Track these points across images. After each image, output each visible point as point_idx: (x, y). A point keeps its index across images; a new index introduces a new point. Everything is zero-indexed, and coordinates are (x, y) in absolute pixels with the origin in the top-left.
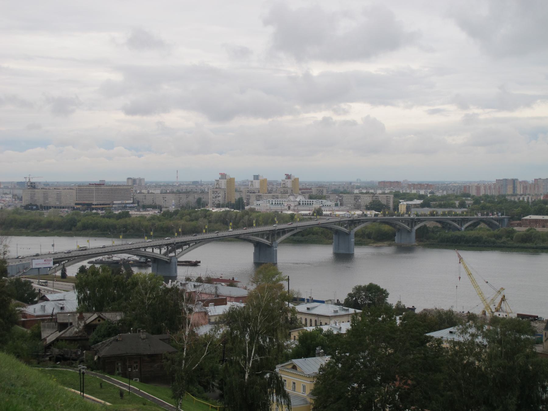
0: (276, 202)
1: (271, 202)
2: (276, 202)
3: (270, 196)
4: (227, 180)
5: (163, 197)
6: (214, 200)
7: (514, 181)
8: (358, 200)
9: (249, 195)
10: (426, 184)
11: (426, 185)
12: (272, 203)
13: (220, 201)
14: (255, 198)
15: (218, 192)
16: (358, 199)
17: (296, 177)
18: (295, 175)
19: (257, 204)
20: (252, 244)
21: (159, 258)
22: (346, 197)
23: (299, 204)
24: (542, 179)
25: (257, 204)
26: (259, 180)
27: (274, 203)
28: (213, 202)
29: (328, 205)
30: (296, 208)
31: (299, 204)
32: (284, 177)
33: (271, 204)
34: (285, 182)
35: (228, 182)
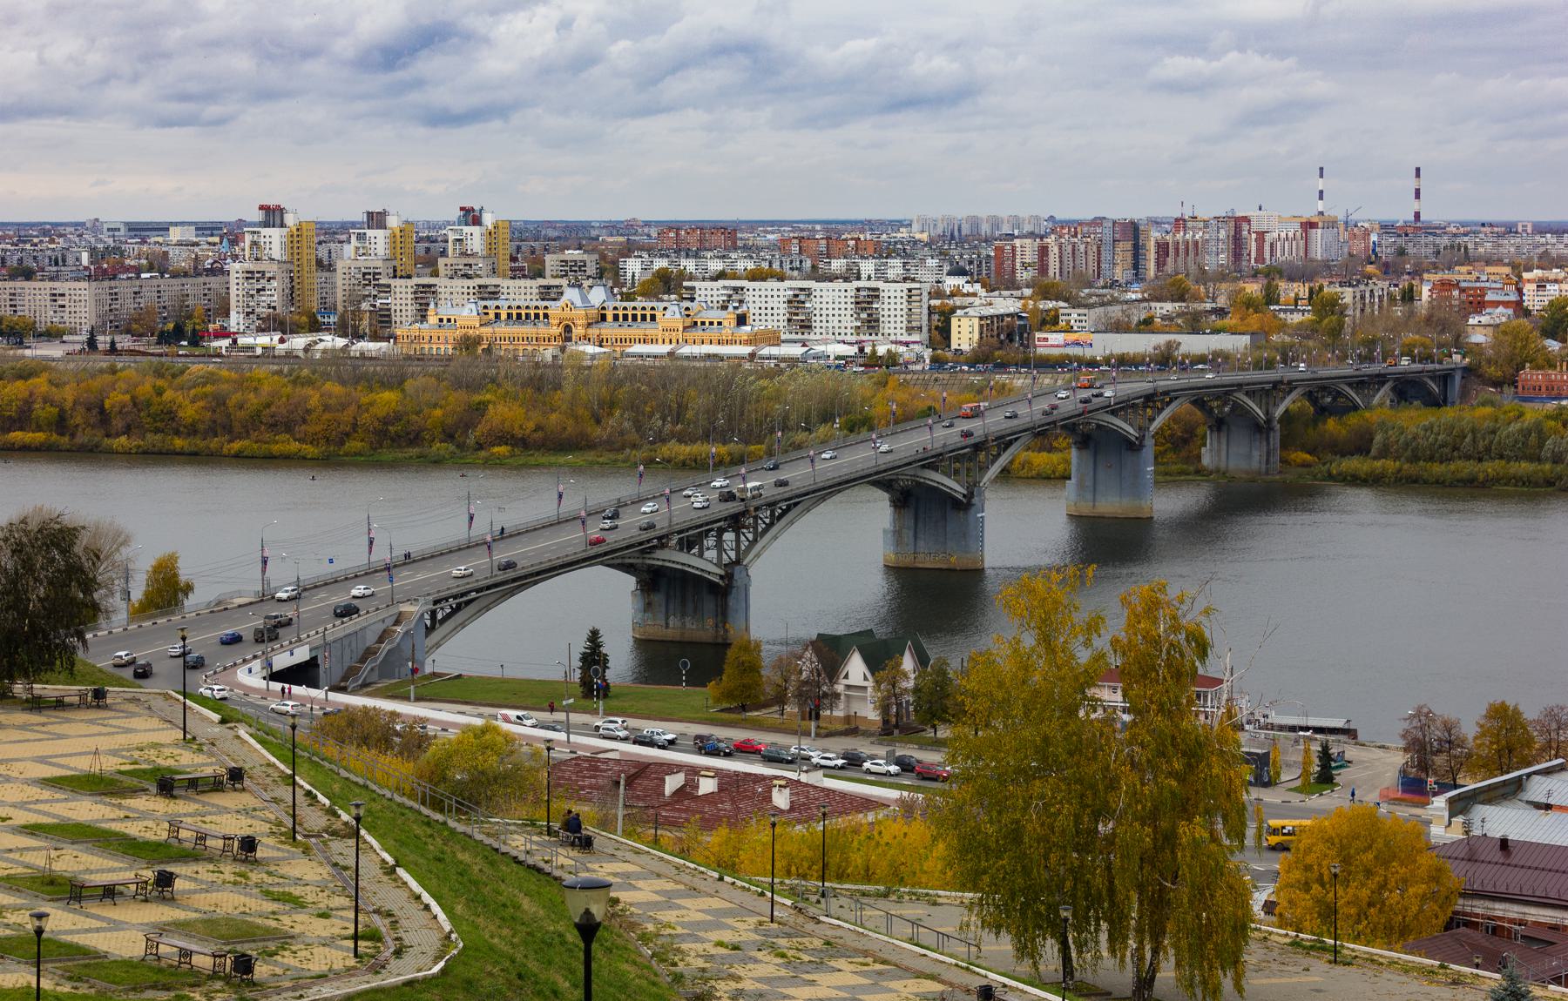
2: (514, 312)
5: (55, 295)
7: (1133, 231)
9: (389, 286)
13: (274, 308)
14: (410, 296)
15: (267, 275)
16: (802, 298)
19: (441, 320)
20: (886, 496)
21: (679, 567)
24: (1204, 213)
25: (441, 320)
26: (282, 225)
30: (593, 332)
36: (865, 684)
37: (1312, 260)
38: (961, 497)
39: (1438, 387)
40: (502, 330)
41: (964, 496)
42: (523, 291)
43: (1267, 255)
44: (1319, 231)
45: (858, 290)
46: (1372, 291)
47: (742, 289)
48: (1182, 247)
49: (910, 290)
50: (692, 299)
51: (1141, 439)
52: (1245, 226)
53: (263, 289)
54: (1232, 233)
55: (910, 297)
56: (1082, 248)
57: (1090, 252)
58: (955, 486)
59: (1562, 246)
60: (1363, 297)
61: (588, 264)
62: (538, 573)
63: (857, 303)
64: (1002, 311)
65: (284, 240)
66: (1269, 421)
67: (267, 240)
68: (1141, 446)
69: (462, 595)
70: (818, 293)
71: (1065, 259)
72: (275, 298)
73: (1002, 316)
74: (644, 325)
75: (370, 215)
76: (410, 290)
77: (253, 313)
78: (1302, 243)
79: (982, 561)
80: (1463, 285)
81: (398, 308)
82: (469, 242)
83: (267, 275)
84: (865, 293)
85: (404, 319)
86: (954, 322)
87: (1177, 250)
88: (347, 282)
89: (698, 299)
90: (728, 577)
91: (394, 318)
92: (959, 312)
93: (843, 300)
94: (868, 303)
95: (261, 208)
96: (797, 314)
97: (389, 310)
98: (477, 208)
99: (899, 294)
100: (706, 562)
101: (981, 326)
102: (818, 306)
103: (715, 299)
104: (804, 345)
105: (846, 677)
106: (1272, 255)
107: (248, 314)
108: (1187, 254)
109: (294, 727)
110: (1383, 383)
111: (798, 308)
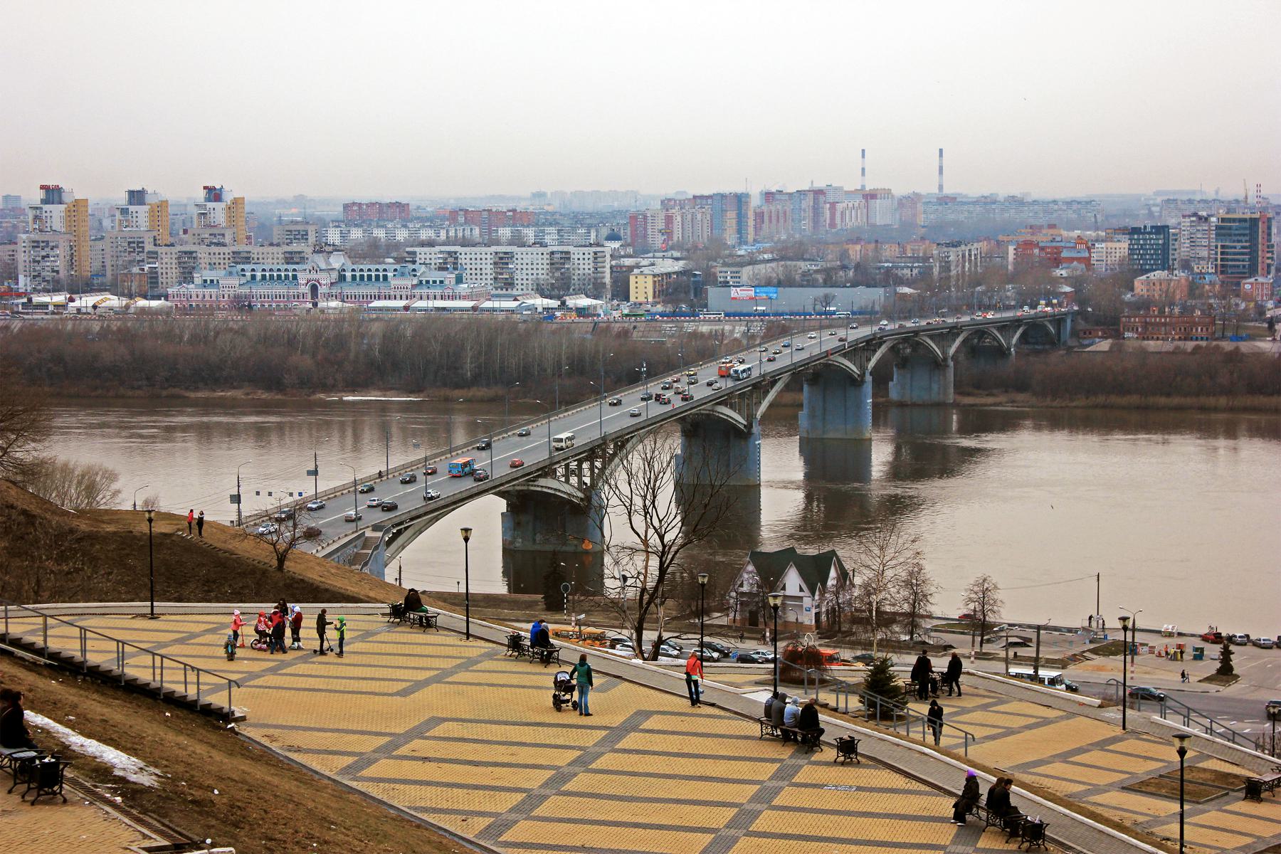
0: (358, 274)
1: (248, 274)
2: (358, 274)
3: (224, 254)
4: (66, 206)
6: (38, 268)
8: (507, 264)
9: (156, 253)
10: (510, 211)
11: (511, 214)
12: (253, 277)
13: (57, 272)
14: (174, 261)
15: (51, 244)
17: (79, 196)
18: (75, 190)
22: (468, 256)
23: (342, 278)
25: (205, 281)
26: (61, 203)
27: (259, 275)
28: (36, 274)
29: (435, 282)
31: (342, 278)
32: (201, 195)
33: (249, 278)
34: (205, 209)
35: (69, 211)
36: (801, 594)
37: (874, 226)
38: (742, 427)
39: (1054, 328)
40: (259, 290)
41: (745, 426)
42: (271, 256)
43: (838, 220)
44: (878, 201)
45: (552, 253)
46: (970, 250)
47: (456, 253)
48: (781, 215)
49: (595, 253)
50: (414, 262)
51: (863, 375)
52: (822, 198)
53: (48, 256)
54: (812, 203)
55: (595, 258)
56: (699, 216)
57: (705, 221)
58: (738, 418)
59: (1071, 212)
60: (964, 256)
61: (310, 233)
62: (455, 503)
63: (552, 264)
64: (670, 270)
65: (63, 214)
66: (945, 359)
67: (48, 214)
68: (863, 382)
69: (401, 523)
70: (519, 256)
71: (686, 226)
72: (58, 264)
73: (669, 273)
74: (377, 285)
75: (131, 193)
76: (174, 256)
77: (39, 275)
78: (865, 210)
79: (759, 480)
80: (1041, 244)
81: (164, 271)
82: (212, 215)
83: (51, 244)
84: (559, 256)
85: (169, 280)
86: (632, 279)
87: (770, 217)
88: (114, 249)
89: (419, 261)
90: (588, 499)
91: (160, 280)
92: (636, 271)
93: (540, 262)
94: (561, 264)
95: (42, 187)
96: (502, 274)
97: (156, 273)
98: (218, 187)
99: (587, 256)
100: (563, 486)
101: (655, 282)
102: (519, 267)
103: (433, 262)
104: (516, 300)
105: (784, 588)
106: (842, 222)
107: (35, 277)
108: (778, 221)
109: (1182, 752)
110: (1019, 327)
111: (503, 268)
